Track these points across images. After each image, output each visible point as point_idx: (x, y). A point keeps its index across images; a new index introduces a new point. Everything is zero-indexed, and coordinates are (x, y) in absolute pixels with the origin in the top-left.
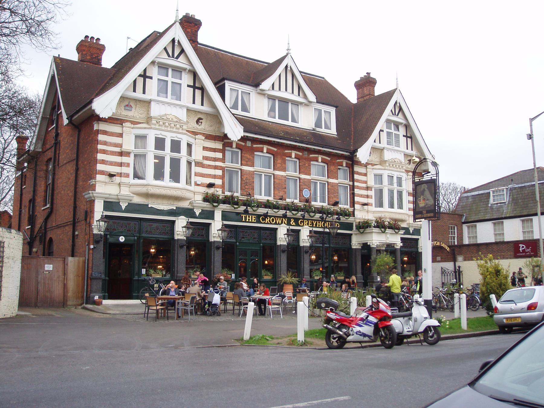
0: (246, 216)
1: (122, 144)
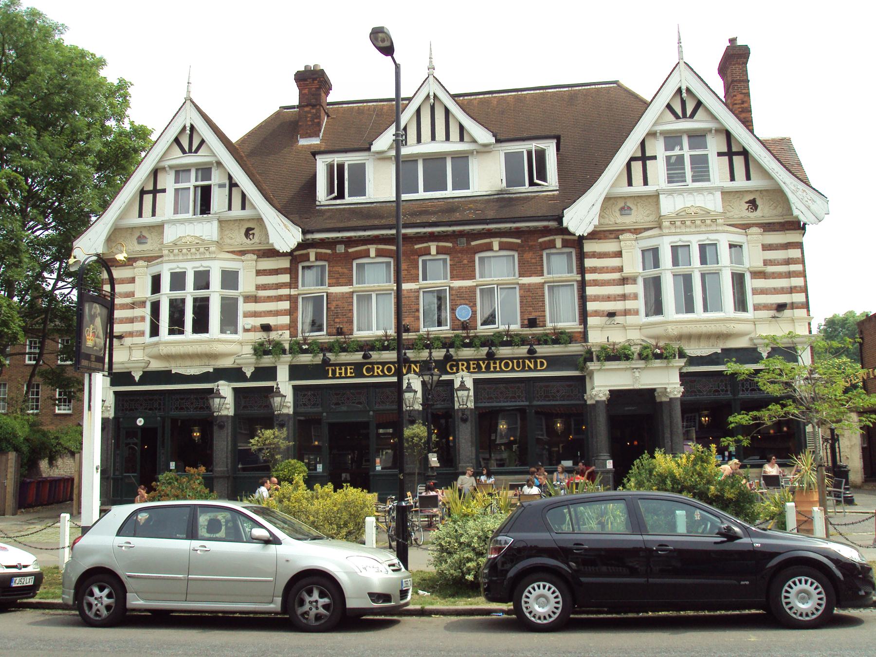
0: (336, 369)
1: (622, 266)
